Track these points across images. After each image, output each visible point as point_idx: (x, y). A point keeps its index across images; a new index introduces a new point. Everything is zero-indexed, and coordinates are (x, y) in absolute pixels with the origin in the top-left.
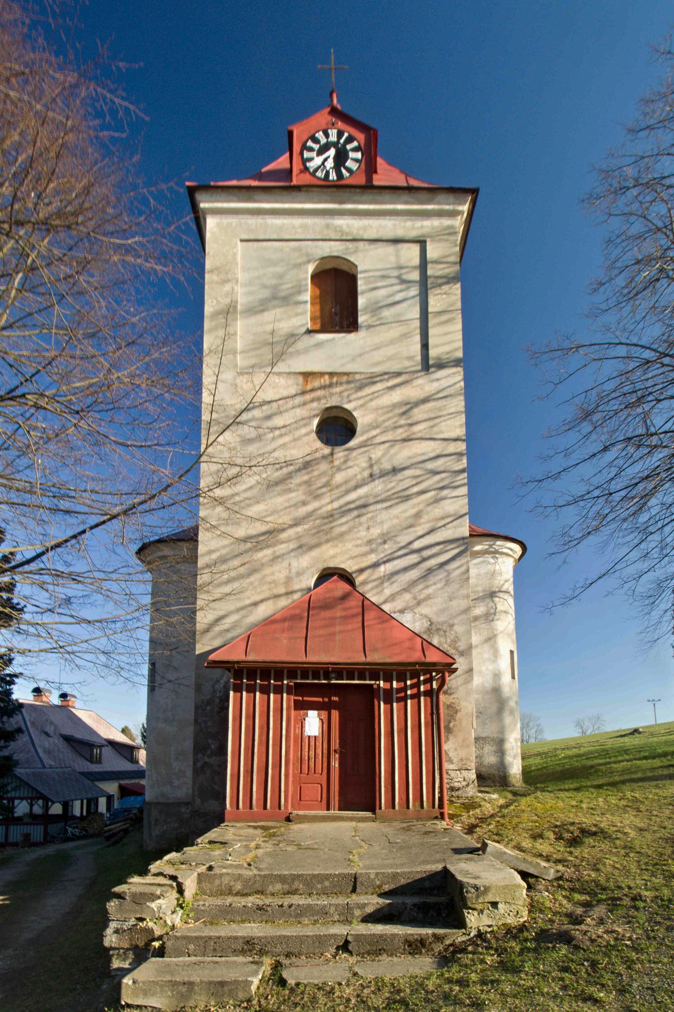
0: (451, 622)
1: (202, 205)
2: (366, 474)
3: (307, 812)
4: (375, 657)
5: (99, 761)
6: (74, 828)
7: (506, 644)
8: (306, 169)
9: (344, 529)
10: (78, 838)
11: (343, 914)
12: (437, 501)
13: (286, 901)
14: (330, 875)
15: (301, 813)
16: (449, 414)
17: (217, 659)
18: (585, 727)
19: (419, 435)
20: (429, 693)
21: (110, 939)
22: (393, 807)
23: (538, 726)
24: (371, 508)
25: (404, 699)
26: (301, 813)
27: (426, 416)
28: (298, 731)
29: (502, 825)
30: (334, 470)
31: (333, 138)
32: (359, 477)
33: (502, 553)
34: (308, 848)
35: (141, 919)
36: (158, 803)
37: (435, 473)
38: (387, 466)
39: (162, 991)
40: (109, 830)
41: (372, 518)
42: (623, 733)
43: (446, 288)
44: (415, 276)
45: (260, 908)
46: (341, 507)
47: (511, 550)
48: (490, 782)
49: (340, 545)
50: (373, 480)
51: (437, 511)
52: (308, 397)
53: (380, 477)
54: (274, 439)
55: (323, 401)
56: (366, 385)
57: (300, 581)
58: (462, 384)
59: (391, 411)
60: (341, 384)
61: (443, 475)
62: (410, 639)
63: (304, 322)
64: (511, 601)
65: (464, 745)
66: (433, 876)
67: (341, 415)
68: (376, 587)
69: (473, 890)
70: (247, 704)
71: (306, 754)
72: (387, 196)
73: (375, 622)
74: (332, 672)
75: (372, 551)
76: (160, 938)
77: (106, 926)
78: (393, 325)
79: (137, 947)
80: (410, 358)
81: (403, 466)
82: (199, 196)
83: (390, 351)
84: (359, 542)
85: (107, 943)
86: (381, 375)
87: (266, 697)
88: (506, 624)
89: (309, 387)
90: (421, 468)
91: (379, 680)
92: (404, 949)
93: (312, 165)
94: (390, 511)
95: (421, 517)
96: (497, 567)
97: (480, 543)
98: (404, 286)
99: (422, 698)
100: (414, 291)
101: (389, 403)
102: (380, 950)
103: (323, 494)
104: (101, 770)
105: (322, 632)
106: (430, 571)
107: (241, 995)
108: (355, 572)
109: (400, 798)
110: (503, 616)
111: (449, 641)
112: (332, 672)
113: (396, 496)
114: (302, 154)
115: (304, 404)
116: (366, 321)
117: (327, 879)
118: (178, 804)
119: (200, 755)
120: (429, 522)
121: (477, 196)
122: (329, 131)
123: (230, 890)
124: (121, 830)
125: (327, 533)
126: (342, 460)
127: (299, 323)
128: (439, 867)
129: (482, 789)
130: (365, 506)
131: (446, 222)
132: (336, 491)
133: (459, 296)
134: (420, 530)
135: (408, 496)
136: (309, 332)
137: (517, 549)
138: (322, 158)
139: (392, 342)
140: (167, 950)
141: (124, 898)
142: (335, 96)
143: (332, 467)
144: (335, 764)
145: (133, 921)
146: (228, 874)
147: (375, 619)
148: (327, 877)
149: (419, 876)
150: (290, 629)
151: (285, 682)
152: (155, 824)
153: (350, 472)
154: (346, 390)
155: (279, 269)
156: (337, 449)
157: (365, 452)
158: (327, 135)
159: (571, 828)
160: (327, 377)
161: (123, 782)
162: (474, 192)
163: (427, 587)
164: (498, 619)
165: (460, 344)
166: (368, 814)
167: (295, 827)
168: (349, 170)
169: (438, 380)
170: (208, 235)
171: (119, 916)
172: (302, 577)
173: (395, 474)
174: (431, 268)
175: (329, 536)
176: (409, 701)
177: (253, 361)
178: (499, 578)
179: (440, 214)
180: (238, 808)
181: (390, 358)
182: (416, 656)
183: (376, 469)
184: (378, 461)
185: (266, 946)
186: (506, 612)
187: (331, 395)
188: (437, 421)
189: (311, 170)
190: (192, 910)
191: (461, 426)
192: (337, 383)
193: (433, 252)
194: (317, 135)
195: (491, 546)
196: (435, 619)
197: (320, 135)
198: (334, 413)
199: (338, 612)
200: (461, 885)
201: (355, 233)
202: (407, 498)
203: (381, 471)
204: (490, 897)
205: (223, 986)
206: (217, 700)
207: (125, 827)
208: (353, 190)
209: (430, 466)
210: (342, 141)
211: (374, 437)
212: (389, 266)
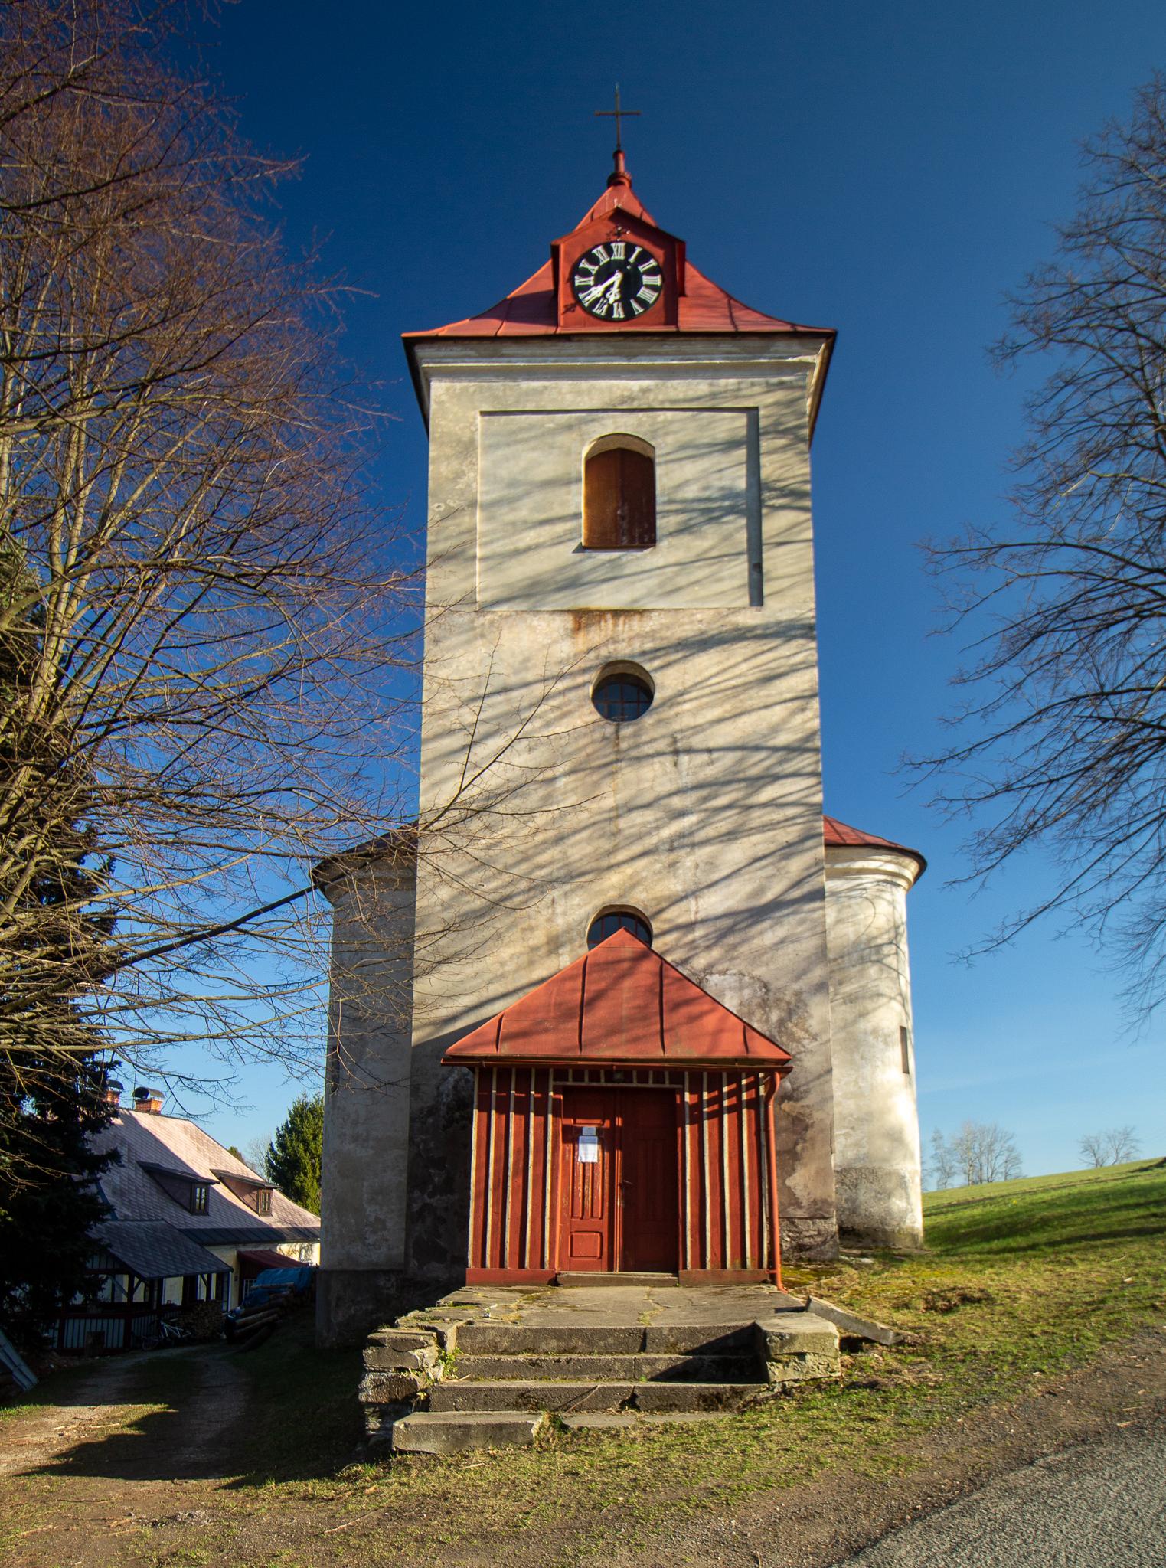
3: (582, 1273)
5: (204, 1211)
6: (173, 1324)
8: (579, 302)
10: (178, 1343)
11: (630, 1371)
13: (564, 1357)
14: (615, 1330)
15: (573, 1273)
18: (1101, 1153)
20: (754, 1104)
22: (703, 1265)
23: (1011, 1150)
25: (718, 1115)
26: (573, 1273)
29: (860, 1294)
35: (404, 1370)
36: (343, 1272)
39: (436, 1435)
40: (245, 1324)
42: (1145, 1166)
45: (533, 1363)
67: (631, 671)
69: (777, 1339)
71: (580, 1189)
72: (699, 345)
74: (617, 1071)
82: (421, 352)
92: (698, 1405)
93: (587, 299)
102: (671, 1405)
104: (209, 1227)
109: (713, 1253)
112: (617, 1071)
114: (571, 280)
117: (611, 1335)
118: (373, 1273)
119: (417, 1194)
122: (613, 245)
123: (496, 1347)
124: (262, 1325)
128: (748, 1323)
138: (601, 288)
140: (433, 1404)
141: (383, 1346)
142: (621, 156)
146: (493, 1328)
148: (611, 1332)
152: (337, 1306)
158: (610, 251)
159: (949, 1295)
161: (243, 1249)
162: (831, 337)
166: (668, 1276)
167: (566, 1293)
168: (642, 303)
170: (433, 407)
171: (376, 1366)
176: (726, 1117)
185: (543, 1400)
189: (586, 305)
190: (455, 1364)
197: (599, 252)
198: (620, 669)
200: (765, 1334)
204: (796, 1348)
205: (501, 1430)
206: (443, 1109)
208: (648, 338)
210: (632, 260)
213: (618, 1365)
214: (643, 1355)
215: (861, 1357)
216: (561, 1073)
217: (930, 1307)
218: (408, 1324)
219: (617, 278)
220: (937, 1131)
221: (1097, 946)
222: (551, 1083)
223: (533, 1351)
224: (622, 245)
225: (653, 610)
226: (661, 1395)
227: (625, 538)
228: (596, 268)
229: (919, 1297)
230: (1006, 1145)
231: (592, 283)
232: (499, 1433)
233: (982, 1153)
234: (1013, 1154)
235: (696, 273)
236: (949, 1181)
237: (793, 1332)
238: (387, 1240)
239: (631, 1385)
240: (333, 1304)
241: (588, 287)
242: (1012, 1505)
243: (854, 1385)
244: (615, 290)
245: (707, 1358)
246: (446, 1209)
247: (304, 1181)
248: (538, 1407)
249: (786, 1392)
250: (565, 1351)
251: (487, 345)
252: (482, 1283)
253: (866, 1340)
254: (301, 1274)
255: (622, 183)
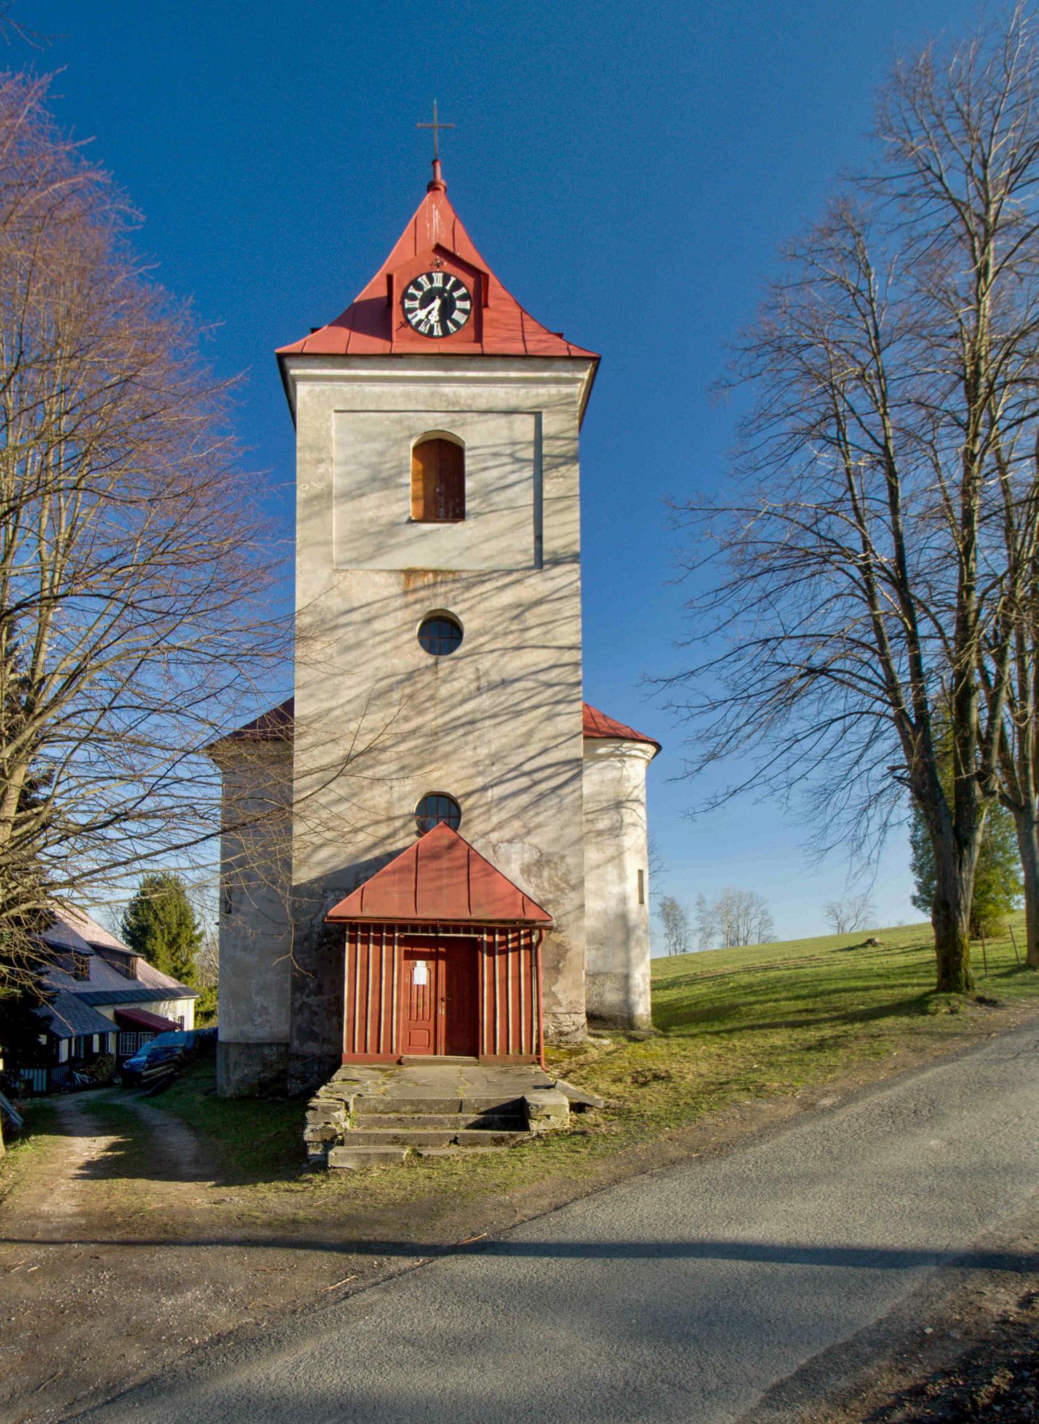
0: (562, 853)
1: (292, 372)
2: (473, 686)
4: (480, 914)
7: (635, 862)
8: (408, 322)
9: (449, 748)
12: (550, 718)
13: (416, 1116)
15: (411, 1056)
16: (564, 619)
17: (336, 915)
18: (843, 917)
19: (531, 643)
20: (529, 947)
21: (308, 1135)
22: (495, 1053)
24: (479, 725)
25: (506, 952)
26: (411, 1056)
27: (539, 621)
28: (408, 980)
30: (438, 682)
31: (438, 283)
32: (465, 690)
33: (630, 756)
34: (424, 1085)
36: (238, 1044)
37: (549, 685)
38: (495, 677)
40: (150, 1076)
41: (479, 737)
43: (563, 469)
44: (529, 453)
45: (399, 1120)
46: (445, 724)
47: (642, 751)
48: (610, 1025)
49: (445, 767)
50: (481, 694)
51: (549, 729)
52: (411, 598)
53: (488, 691)
54: (374, 646)
55: (427, 603)
56: (474, 585)
57: (402, 806)
58: (579, 583)
59: (500, 615)
60: (446, 583)
61: (557, 689)
62: (513, 894)
63: (405, 509)
64: (641, 811)
65: (575, 984)
66: (517, 1101)
68: (484, 813)
70: (362, 955)
72: (499, 362)
73: (479, 875)
75: (480, 774)
76: (341, 1134)
77: (304, 1128)
78: (505, 512)
79: (325, 1140)
80: (525, 551)
81: (514, 677)
82: (288, 362)
83: (502, 543)
84: (465, 763)
85: (306, 1138)
86: (490, 573)
87: (379, 948)
88: (635, 839)
89: (411, 587)
90: (533, 680)
91: (482, 933)
94: (498, 729)
95: (531, 737)
96: (625, 773)
97: (603, 746)
98: (516, 466)
99: (522, 952)
100: (529, 472)
101: (499, 606)
103: (427, 709)
104: (91, 990)
105: (429, 885)
106: (542, 796)
107: (397, 1161)
108: (461, 797)
109: (501, 1044)
110: (630, 830)
111: (560, 874)
113: (505, 712)
114: (402, 303)
115: (407, 606)
116: (474, 508)
118: (259, 1045)
119: (298, 995)
120: (540, 740)
121: (598, 363)
122: (434, 274)
124: (163, 1076)
125: (431, 753)
126: (447, 671)
127: (401, 510)
129: (594, 1032)
130: (472, 722)
131: (566, 389)
132: (440, 706)
133: (577, 480)
134: (532, 750)
135: (518, 712)
136: (410, 521)
137: (651, 749)
138: (425, 312)
139: (502, 533)
142: (438, 164)
143: (436, 679)
144: (442, 1012)
145: (322, 1125)
147: (479, 872)
148: (442, 1102)
149: (504, 1102)
150: (400, 881)
151: (397, 935)
152: (235, 1068)
153: (457, 685)
154: (452, 590)
155: (376, 446)
156: (442, 658)
157: (472, 662)
158: (431, 280)
159: (647, 1074)
160: (431, 576)
161: (119, 1008)
163: (538, 814)
164: (625, 834)
165: (577, 536)
166: (472, 1059)
167: (408, 1070)
168: (456, 323)
169: (552, 579)
170: (299, 406)
172: (403, 803)
173: (505, 688)
174: (547, 446)
175: (433, 757)
176: (510, 954)
177: (350, 555)
178: (627, 785)
179: (558, 381)
180: (354, 1052)
181: (502, 552)
182: (516, 913)
183: (483, 682)
184: (487, 673)
186: (634, 825)
187: (435, 596)
188: (550, 626)
191: (577, 633)
192: (442, 582)
193: (549, 426)
194: (419, 280)
195: (617, 749)
196: (545, 848)
197: (423, 280)
198: (438, 614)
199: (444, 863)
200: (528, 1105)
201: (464, 403)
202: (518, 714)
203: (489, 684)
204: (545, 1112)
206: (315, 936)
207: (169, 1071)
209: (543, 677)
210: (448, 287)
211: (482, 645)
212: (499, 442)
213: (446, 1121)
214: (460, 1115)
215: (582, 1115)
217: (635, 1081)
218: (323, 1097)
219: (437, 303)
220: (701, 896)
221: (785, 809)
223: (397, 1112)
224: (440, 275)
226: (472, 1137)
227: (442, 510)
228: (421, 293)
229: (629, 1075)
230: (761, 909)
231: (418, 306)
232: (385, 1157)
233: (739, 917)
234: (766, 918)
235: (497, 283)
236: (710, 940)
237: (543, 1103)
239: (455, 1132)
240: (232, 1066)
241: (415, 309)
242: (628, 1190)
243: (575, 1133)
244: (435, 313)
245: (496, 1116)
246: (318, 1006)
247: (155, 945)
248: (404, 1144)
249: (539, 1136)
250: (416, 1112)
251: (341, 360)
252: (355, 1061)
253: (589, 1105)
254: (188, 1037)
255: (438, 189)
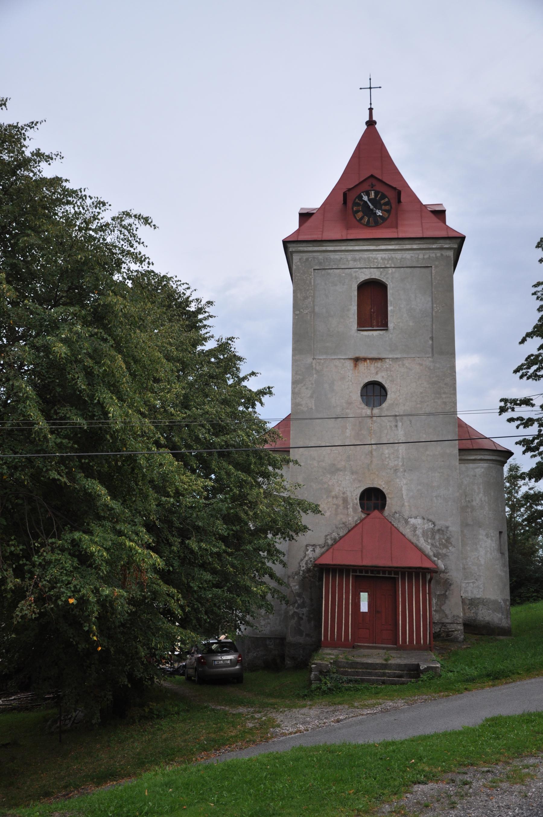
206: (301, 572)
216: (354, 571)
222: (351, 574)
225: (388, 358)
238: (269, 624)
